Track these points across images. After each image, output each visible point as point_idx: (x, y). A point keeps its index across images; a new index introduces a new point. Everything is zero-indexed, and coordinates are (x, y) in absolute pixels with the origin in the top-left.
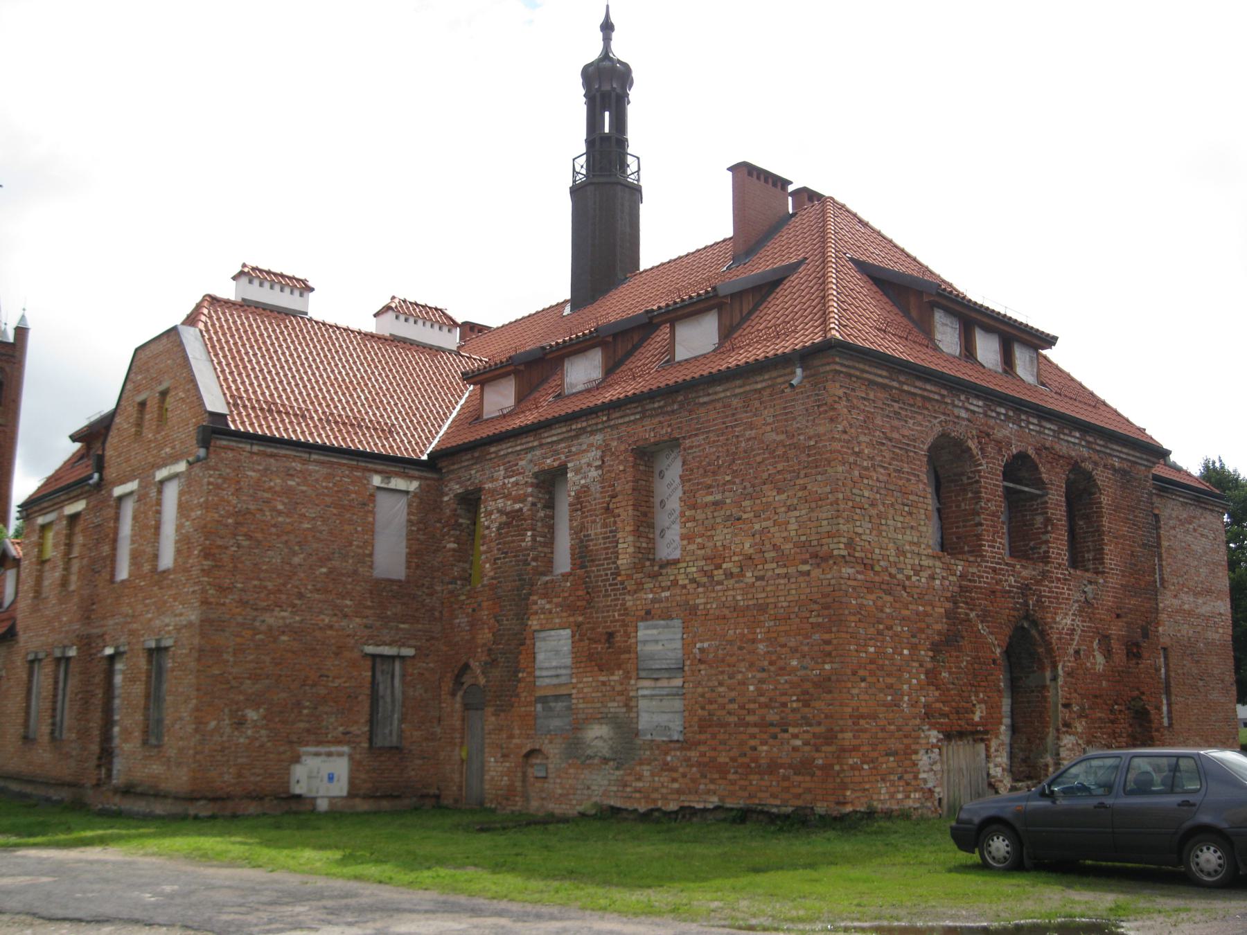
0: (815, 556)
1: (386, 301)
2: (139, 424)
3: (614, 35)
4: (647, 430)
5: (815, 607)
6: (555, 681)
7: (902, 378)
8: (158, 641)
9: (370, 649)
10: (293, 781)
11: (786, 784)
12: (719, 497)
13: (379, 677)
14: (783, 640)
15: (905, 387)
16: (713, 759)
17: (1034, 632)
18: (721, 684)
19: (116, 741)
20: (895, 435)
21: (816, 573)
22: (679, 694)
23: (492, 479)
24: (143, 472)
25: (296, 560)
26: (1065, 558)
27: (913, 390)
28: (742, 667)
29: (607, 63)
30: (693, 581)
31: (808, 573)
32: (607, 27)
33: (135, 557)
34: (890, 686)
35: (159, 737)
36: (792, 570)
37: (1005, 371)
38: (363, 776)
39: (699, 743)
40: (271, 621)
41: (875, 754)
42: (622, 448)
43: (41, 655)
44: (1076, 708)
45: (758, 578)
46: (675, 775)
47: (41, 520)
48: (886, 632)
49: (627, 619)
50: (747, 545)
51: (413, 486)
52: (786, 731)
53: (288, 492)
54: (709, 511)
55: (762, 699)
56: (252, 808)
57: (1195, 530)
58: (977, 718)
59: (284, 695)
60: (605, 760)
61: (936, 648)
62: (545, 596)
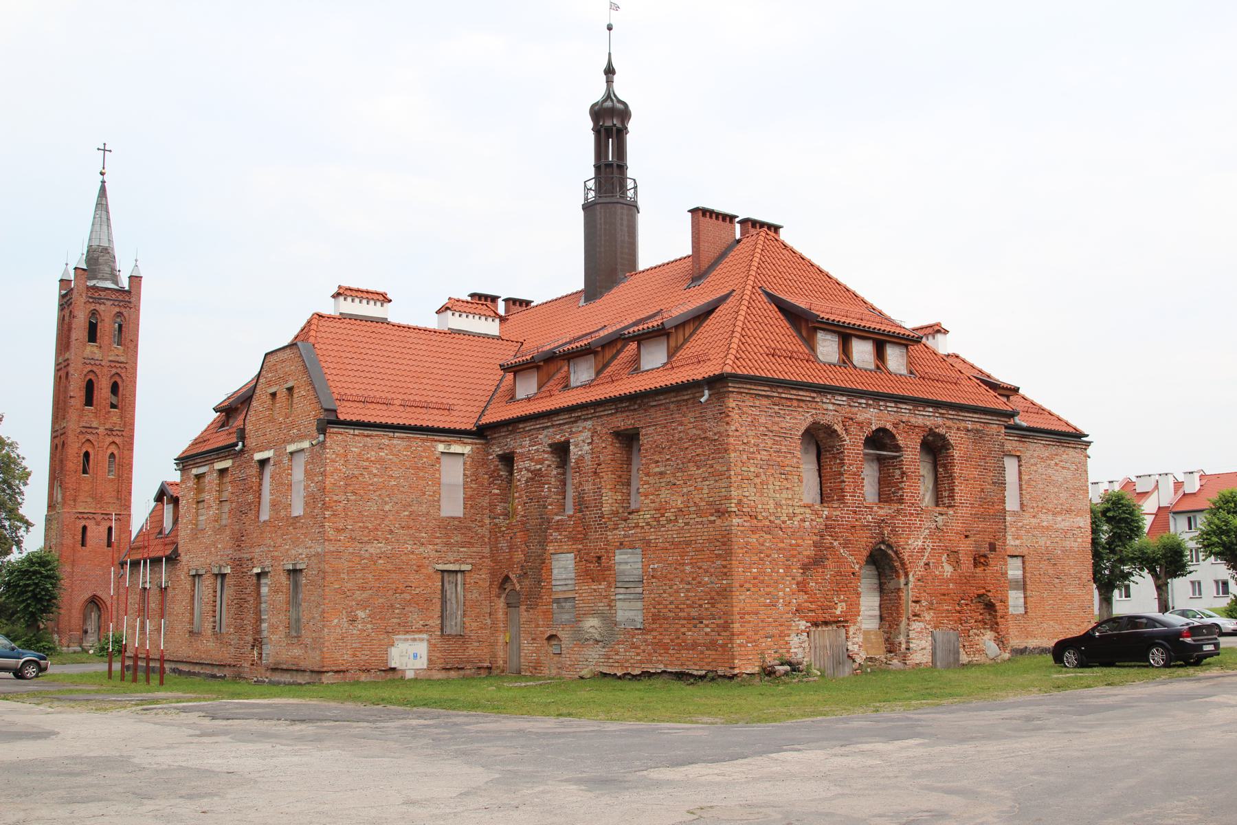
0: (718, 511)
1: (444, 301)
4: (622, 422)
6: (565, 588)
9: (440, 567)
13: (447, 586)
17: (890, 552)
19: (265, 634)
20: (775, 428)
21: (718, 522)
23: (522, 447)
24: (278, 445)
25: (387, 508)
26: (928, 500)
28: (677, 581)
29: (608, 104)
30: (648, 524)
32: (610, 71)
33: (274, 505)
35: (298, 630)
37: (878, 367)
38: (438, 655)
39: (653, 630)
40: (372, 550)
41: (757, 637)
42: (605, 430)
44: (924, 603)
47: (195, 471)
51: (467, 450)
53: (381, 461)
56: (364, 677)
57: (1056, 464)
58: (838, 612)
59: (381, 600)
61: (805, 568)
62: (557, 530)
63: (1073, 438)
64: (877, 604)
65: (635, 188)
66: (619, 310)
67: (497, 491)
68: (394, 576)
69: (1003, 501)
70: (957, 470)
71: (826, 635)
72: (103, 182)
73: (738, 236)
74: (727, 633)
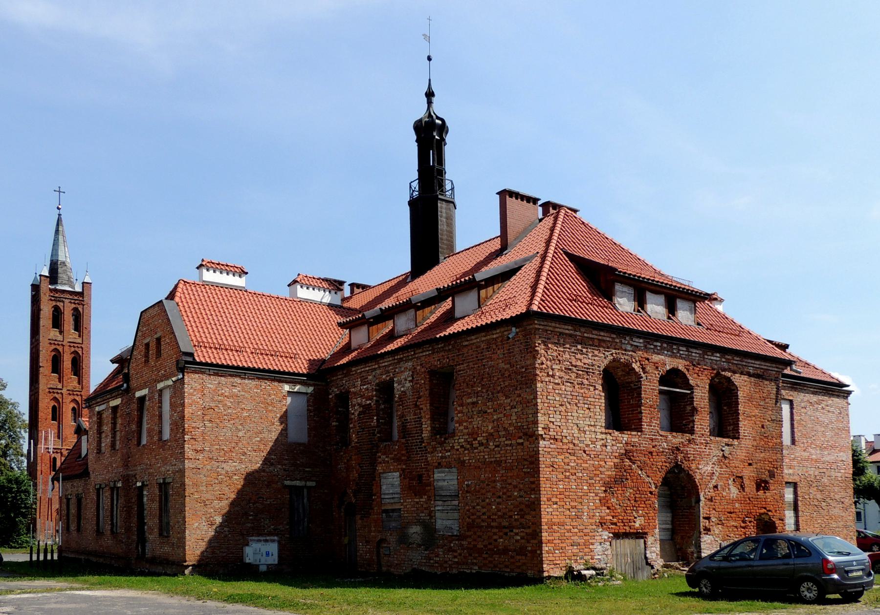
0: (525, 434)
2: (147, 355)
3: (434, 100)
5: (526, 463)
6: (392, 501)
7: (583, 330)
8: (164, 479)
9: (287, 483)
10: (245, 555)
11: (512, 560)
12: (475, 400)
14: (509, 481)
15: (586, 335)
16: (475, 546)
18: (478, 505)
20: (579, 363)
21: (526, 444)
22: (455, 509)
24: (151, 384)
27: (591, 336)
28: (489, 495)
30: (462, 447)
31: (522, 444)
32: (430, 95)
34: (574, 507)
35: (168, 532)
36: (514, 442)
41: (564, 545)
42: (423, 370)
43: (103, 486)
45: (496, 446)
46: (455, 554)
48: (571, 477)
49: (429, 467)
50: (490, 428)
52: (512, 531)
54: (470, 407)
55: (499, 513)
57: (823, 408)
58: (637, 525)
60: (419, 546)
61: (608, 487)
63: (836, 390)
64: (669, 519)
65: (452, 189)
69: (781, 436)
70: (741, 407)
71: (627, 545)
72: (59, 215)
73: (541, 216)
74: (536, 541)
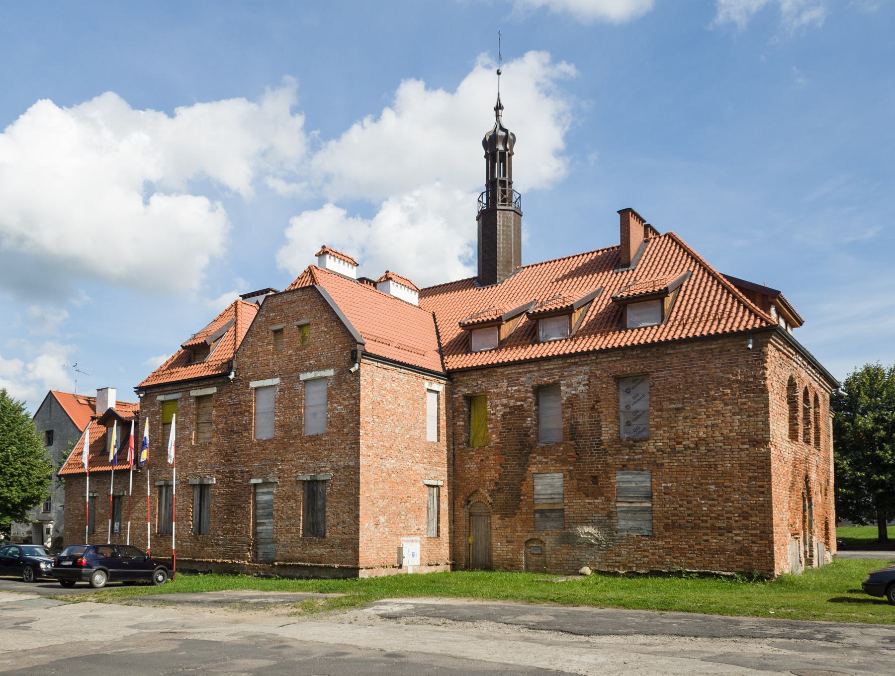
12: (680, 406)
32: (499, 108)
42: (605, 375)
49: (608, 469)
53: (393, 391)
55: (713, 515)
59: (394, 508)
66: (505, 299)
67: (462, 423)
68: (401, 488)
